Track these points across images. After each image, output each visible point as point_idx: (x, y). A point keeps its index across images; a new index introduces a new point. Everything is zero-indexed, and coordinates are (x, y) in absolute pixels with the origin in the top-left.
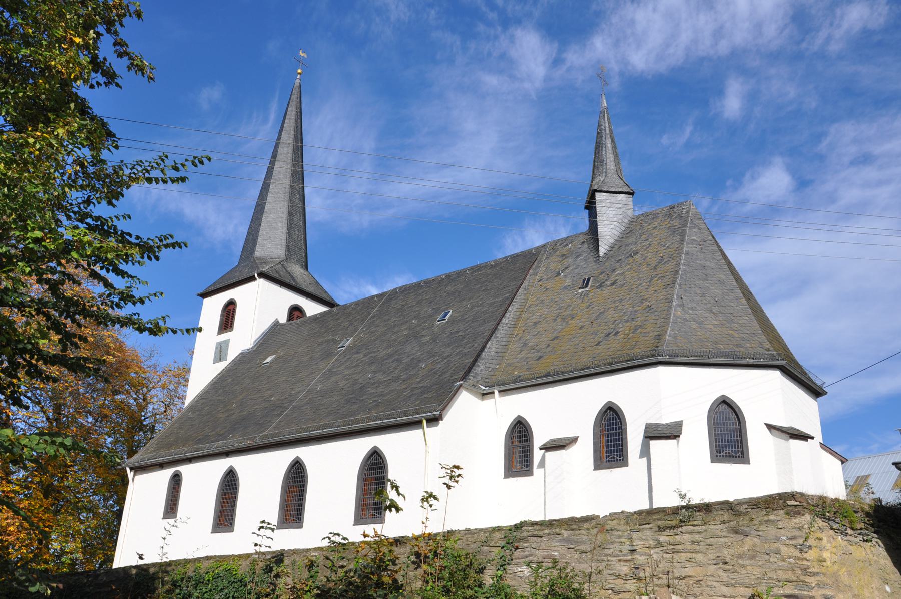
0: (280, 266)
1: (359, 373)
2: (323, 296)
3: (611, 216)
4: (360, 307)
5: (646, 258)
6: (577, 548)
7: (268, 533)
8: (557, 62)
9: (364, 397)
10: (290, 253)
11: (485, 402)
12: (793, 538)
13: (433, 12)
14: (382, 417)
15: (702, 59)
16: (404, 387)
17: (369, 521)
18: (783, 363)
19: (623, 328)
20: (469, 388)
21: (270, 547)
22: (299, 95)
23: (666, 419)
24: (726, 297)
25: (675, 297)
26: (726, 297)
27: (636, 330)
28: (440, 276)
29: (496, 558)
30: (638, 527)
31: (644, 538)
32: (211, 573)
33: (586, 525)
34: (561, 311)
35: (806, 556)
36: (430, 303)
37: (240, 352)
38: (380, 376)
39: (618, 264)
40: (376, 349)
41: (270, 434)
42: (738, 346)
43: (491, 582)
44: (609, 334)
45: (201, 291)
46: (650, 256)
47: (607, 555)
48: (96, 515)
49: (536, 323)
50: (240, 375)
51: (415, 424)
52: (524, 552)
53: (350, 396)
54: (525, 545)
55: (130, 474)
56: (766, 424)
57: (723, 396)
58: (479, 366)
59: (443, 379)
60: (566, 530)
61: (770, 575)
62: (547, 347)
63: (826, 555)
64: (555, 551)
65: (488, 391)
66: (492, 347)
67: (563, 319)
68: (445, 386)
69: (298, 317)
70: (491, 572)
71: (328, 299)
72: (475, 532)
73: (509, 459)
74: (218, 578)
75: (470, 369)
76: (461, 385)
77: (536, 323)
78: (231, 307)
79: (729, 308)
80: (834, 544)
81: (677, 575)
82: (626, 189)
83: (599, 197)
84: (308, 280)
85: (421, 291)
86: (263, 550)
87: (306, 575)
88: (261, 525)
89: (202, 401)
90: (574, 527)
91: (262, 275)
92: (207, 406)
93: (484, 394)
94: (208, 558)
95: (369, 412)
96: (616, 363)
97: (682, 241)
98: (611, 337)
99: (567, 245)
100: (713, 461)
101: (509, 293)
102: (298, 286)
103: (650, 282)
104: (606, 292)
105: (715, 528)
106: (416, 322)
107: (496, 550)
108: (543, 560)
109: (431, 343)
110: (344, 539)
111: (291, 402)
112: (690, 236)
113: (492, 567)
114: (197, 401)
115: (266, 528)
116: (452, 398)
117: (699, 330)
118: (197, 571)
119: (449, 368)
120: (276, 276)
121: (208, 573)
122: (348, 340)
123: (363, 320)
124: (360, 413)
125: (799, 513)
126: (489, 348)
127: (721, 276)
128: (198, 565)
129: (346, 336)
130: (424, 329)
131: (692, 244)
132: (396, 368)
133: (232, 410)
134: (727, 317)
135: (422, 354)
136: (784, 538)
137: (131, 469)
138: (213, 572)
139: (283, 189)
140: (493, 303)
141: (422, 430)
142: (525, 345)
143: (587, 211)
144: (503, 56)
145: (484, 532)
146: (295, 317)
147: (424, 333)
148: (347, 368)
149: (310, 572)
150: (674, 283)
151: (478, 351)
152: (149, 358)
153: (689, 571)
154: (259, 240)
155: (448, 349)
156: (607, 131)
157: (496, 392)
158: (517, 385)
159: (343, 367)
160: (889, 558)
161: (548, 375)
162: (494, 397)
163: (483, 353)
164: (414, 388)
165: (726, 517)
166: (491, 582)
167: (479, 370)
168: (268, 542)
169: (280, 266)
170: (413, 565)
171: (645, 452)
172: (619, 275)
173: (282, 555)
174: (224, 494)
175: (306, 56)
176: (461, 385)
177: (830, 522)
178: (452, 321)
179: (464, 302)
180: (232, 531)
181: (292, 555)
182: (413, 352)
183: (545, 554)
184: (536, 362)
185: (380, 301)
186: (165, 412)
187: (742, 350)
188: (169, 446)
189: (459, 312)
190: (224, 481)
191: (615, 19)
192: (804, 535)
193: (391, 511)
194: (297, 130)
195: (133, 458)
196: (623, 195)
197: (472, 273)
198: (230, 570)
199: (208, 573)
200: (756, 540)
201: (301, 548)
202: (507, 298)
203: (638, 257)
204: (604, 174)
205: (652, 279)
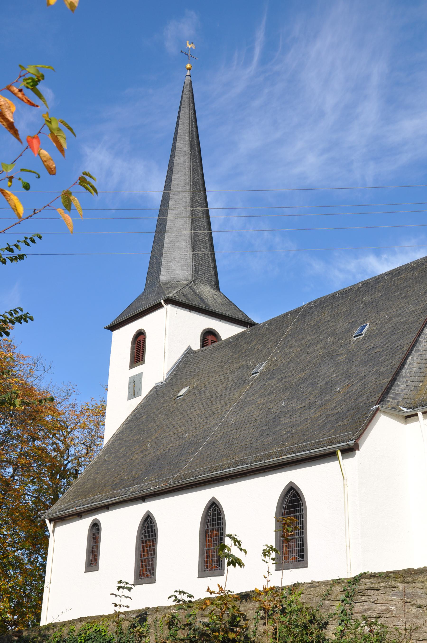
0: (187, 288)
1: (273, 401)
4: (273, 327)
6: (413, 602)
7: (126, 592)
10: (197, 273)
11: (409, 425)
14: (294, 450)
16: (319, 413)
17: (291, 565)
20: (388, 411)
21: (128, 607)
22: (190, 94)
28: (357, 285)
29: (337, 612)
32: (83, 635)
36: (346, 316)
37: (154, 385)
38: (295, 404)
40: (290, 374)
41: (183, 475)
45: (108, 324)
50: (154, 411)
52: (364, 606)
53: (264, 428)
54: (364, 598)
55: (50, 526)
58: (399, 386)
59: (359, 404)
60: (401, 583)
64: (392, 605)
65: (411, 414)
68: (360, 411)
69: (213, 342)
70: (333, 627)
71: (243, 318)
72: (317, 584)
74: (89, 639)
75: (388, 390)
76: (377, 409)
78: (141, 338)
84: (219, 300)
85: (337, 303)
86: (123, 610)
88: (119, 585)
89: (117, 443)
90: (409, 579)
92: (123, 447)
93: (407, 417)
94: (81, 620)
95: (283, 445)
102: (209, 309)
106: (332, 340)
107: (337, 604)
108: (382, 615)
109: (347, 363)
110: (190, 596)
111: (205, 437)
113: (334, 622)
115: (124, 588)
116: (370, 421)
118: (71, 634)
119: (366, 390)
120: (184, 300)
121: (80, 635)
122: (261, 365)
123: (277, 341)
124: (273, 446)
126: (410, 363)
128: (72, 627)
129: (259, 360)
130: (340, 347)
132: (310, 394)
133: (147, 450)
135: (337, 376)
137: (50, 521)
138: (85, 634)
140: (414, 312)
141: (338, 462)
145: (326, 585)
146: (209, 342)
147: (340, 351)
148: (261, 397)
149: (170, 630)
151: (396, 369)
152: (67, 398)
154: (164, 262)
155: (365, 368)
157: (420, 414)
159: (256, 396)
162: (418, 420)
163: (403, 371)
167: (400, 390)
169: (187, 288)
170: (262, 621)
173: (146, 613)
174: (144, 542)
175: (194, 47)
176: (377, 409)
178: (369, 336)
179: (382, 313)
180: (154, 582)
181: (155, 612)
182: (328, 374)
183: (383, 608)
185: (293, 318)
186: (87, 454)
188: (86, 493)
189: (377, 324)
190: (142, 528)
193: (235, 566)
194: (193, 135)
195: (51, 509)
197: (391, 278)
198: (99, 630)
199: (80, 635)
201: (164, 605)
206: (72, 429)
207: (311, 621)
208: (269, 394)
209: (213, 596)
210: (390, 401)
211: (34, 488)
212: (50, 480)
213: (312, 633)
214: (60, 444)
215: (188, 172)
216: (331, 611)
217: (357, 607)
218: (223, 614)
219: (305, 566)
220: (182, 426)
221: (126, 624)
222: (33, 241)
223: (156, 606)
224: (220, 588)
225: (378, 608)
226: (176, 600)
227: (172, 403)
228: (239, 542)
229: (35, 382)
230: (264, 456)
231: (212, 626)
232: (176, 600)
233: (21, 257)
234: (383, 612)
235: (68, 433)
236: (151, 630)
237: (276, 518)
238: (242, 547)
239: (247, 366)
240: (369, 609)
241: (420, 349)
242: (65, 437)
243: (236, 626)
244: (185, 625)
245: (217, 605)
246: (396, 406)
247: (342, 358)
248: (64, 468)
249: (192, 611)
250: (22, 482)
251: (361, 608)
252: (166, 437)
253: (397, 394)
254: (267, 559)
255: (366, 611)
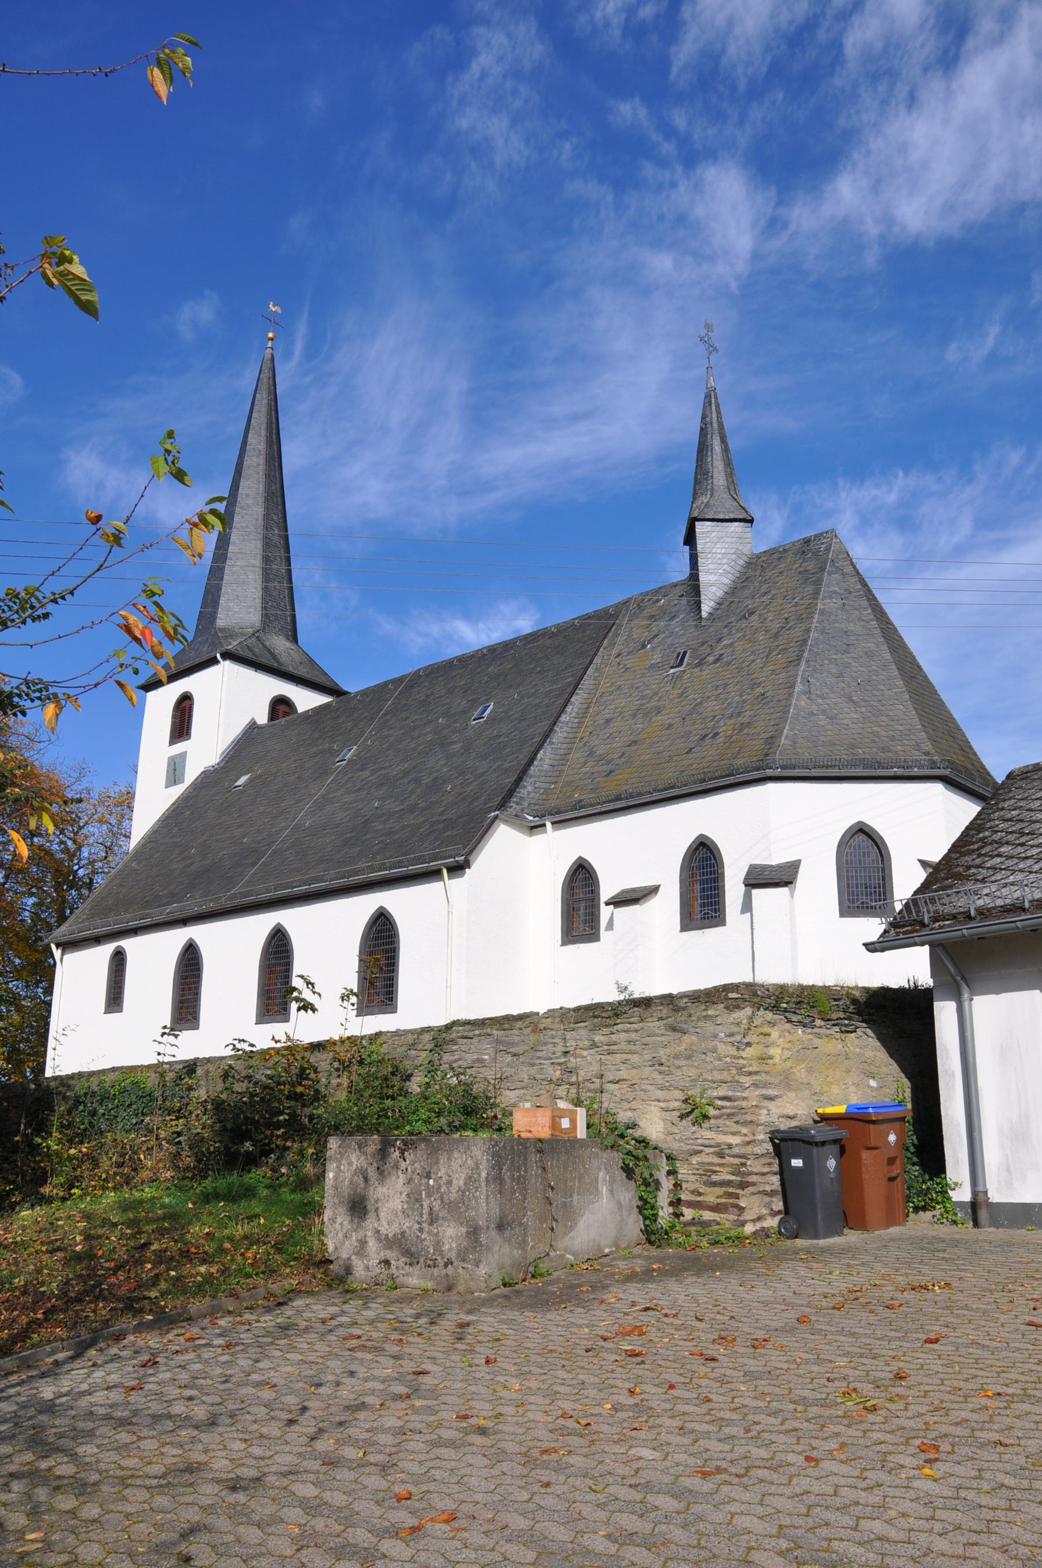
2: (321, 680)
3: (719, 556)
5: (765, 619)
8: (773, 225)
9: (368, 836)
11: (534, 838)
12: (731, 1035)
13: (567, 147)
15: (1021, 208)
17: (376, 1009)
18: (947, 772)
19: (725, 727)
20: (510, 820)
23: (777, 858)
24: (874, 677)
25: (799, 680)
26: (874, 677)
27: (741, 730)
30: (572, 1025)
31: (580, 1035)
33: (519, 1024)
34: (644, 701)
35: (743, 1054)
37: (202, 770)
38: (391, 805)
39: (726, 630)
40: (387, 764)
42: (884, 749)
43: (419, 1090)
44: (706, 736)
46: (770, 616)
47: (539, 1058)
48: (19, 1009)
49: (608, 721)
51: (432, 875)
53: (349, 835)
54: (455, 1047)
55: (57, 953)
56: (919, 861)
57: (860, 822)
58: (525, 787)
61: (705, 1076)
62: (620, 757)
63: (774, 1051)
64: (486, 1054)
66: (545, 757)
67: (645, 715)
69: (286, 714)
71: (328, 684)
73: (568, 920)
75: (511, 793)
76: (496, 817)
77: (608, 721)
78: (186, 703)
79: (877, 693)
80: (789, 1037)
81: (611, 1078)
82: (742, 515)
83: (700, 527)
84: (297, 657)
85: (454, 673)
86: (167, 1059)
87: (220, 1086)
90: (506, 1026)
91: (227, 656)
93: (532, 828)
94: (114, 1070)
96: (710, 780)
97: (817, 593)
98: (708, 741)
99: (658, 600)
100: (842, 914)
101: (572, 676)
102: (283, 668)
103: (767, 656)
104: (707, 672)
105: (653, 1025)
107: (424, 1054)
110: (252, 1045)
111: (270, 844)
112: (828, 586)
114: (144, 845)
116: (486, 832)
117: (829, 727)
120: (249, 655)
123: (372, 719)
125: (738, 1007)
127: (869, 645)
129: (347, 744)
131: (831, 598)
132: (412, 792)
134: (872, 706)
135: (449, 771)
136: (722, 1035)
137: (58, 946)
139: (254, 522)
140: (550, 692)
142: (592, 753)
143: (687, 548)
144: (682, 219)
146: (281, 714)
147: (454, 738)
150: (799, 658)
152: (78, 780)
153: (623, 1074)
154: (222, 601)
156: (715, 425)
157: (549, 825)
158: (576, 814)
160: (883, 1049)
161: (618, 798)
162: (546, 832)
163: (532, 768)
164: (435, 822)
165: (665, 1012)
166: (419, 1090)
168: (170, 1050)
171: (747, 906)
172: (726, 647)
173: (195, 1064)
174: (184, 978)
175: (279, 311)
176: (496, 817)
177: (787, 1014)
178: (493, 719)
179: (511, 691)
184: (605, 779)
185: (396, 689)
186: (106, 858)
187: (890, 754)
188: (106, 912)
191: (876, 144)
192: (742, 1030)
194: (271, 428)
196: (736, 524)
197: (525, 645)
200: (694, 1038)
202: (569, 684)
203: (754, 618)
204: (709, 493)
205: (769, 653)
206: (86, 823)
207: (393, 1074)
208: (358, 790)
209: (279, 1045)
210: (513, 806)
211: (31, 901)
212: (55, 890)
213: (393, 1086)
214: (70, 843)
215: (262, 479)
216: (417, 1063)
217: (447, 1057)
218: (289, 1066)
219: (394, 1010)
220: (240, 827)
221: (169, 1076)
222: (63, 598)
223: (207, 1056)
224: (288, 1037)
225: (470, 1057)
226: (234, 1048)
227: (227, 795)
228: (313, 984)
229: (36, 757)
230: (348, 871)
231: (275, 1079)
232: (234, 1048)
233: (46, 616)
234: (474, 1061)
235: (80, 828)
236: (202, 1083)
237: (360, 956)
238: (316, 990)
239: (330, 750)
240: (460, 1059)
241: (554, 741)
242: (76, 834)
243: (305, 1079)
244: (245, 1077)
245: (283, 1056)
246: (519, 814)
247: (456, 747)
248: (74, 877)
249: (252, 1062)
250: (16, 892)
251: (451, 1058)
252: (217, 841)
253: (521, 798)
254: (345, 1003)
255: (456, 1061)
